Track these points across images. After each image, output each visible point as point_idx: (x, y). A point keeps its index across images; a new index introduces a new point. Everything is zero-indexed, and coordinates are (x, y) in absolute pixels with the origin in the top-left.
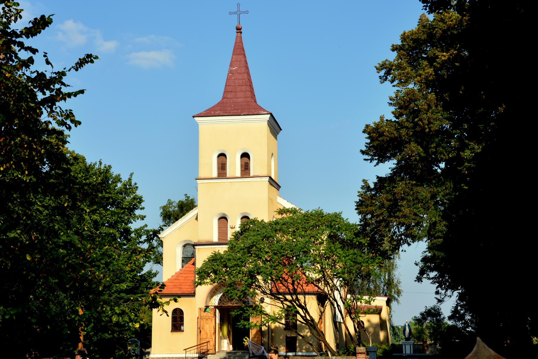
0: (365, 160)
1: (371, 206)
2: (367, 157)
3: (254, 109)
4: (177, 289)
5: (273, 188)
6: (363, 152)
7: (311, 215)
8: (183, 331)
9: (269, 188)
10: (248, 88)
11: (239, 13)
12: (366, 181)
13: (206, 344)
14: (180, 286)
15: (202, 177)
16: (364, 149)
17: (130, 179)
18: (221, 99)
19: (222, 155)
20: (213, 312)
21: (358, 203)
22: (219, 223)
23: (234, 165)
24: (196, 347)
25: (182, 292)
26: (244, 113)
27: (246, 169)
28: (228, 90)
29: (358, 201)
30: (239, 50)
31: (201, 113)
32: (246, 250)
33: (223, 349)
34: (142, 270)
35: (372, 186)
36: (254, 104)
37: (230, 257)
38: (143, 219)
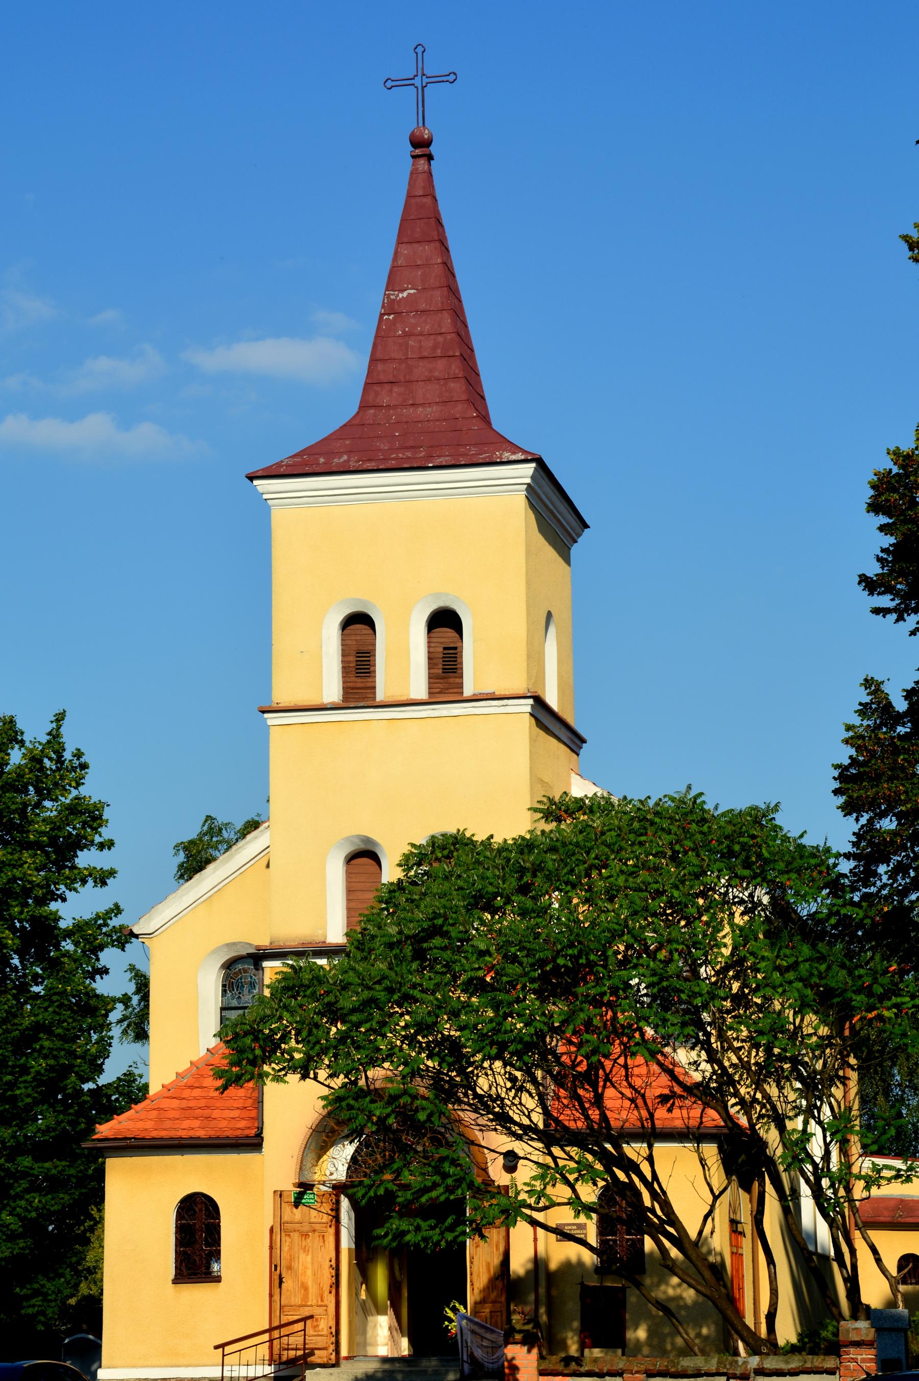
0: (877, 611)
1: (891, 779)
2: (886, 601)
3: (476, 445)
4: (196, 1123)
5: (554, 741)
6: (870, 585)
7: (657, 814)
8: (218, 1279)
9: (533, 741)
10: (456, 368)
11: (420, 82)
12: (879, 684)
13: (300, 1326)
14: (206, 1112)
15: (284, 704)
16: (873, 569)
17: (55, 736)
18: (355, 409)
19: (359, 622)
20: (326, 1208)
21: (846, 768)
22: (349, 874)
23: (404, 658)
24: (266, 1337)
25: (212, 1133)
26: (438, 461)
27: (446, 671)
28: (382, 378)
29: (847, 762)
30: (422, 222)
31: (279, 465)
32: (408, 950)
33: (371, 1351)
34: (100, 1070)
35: (901, 705)
36: (476, 426)
37: (351, 977)
38: (104, 883)
